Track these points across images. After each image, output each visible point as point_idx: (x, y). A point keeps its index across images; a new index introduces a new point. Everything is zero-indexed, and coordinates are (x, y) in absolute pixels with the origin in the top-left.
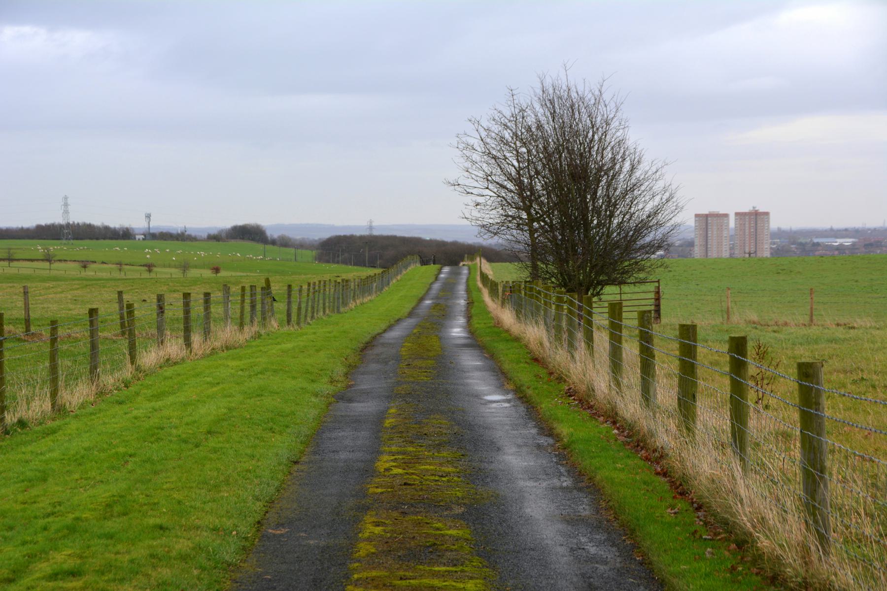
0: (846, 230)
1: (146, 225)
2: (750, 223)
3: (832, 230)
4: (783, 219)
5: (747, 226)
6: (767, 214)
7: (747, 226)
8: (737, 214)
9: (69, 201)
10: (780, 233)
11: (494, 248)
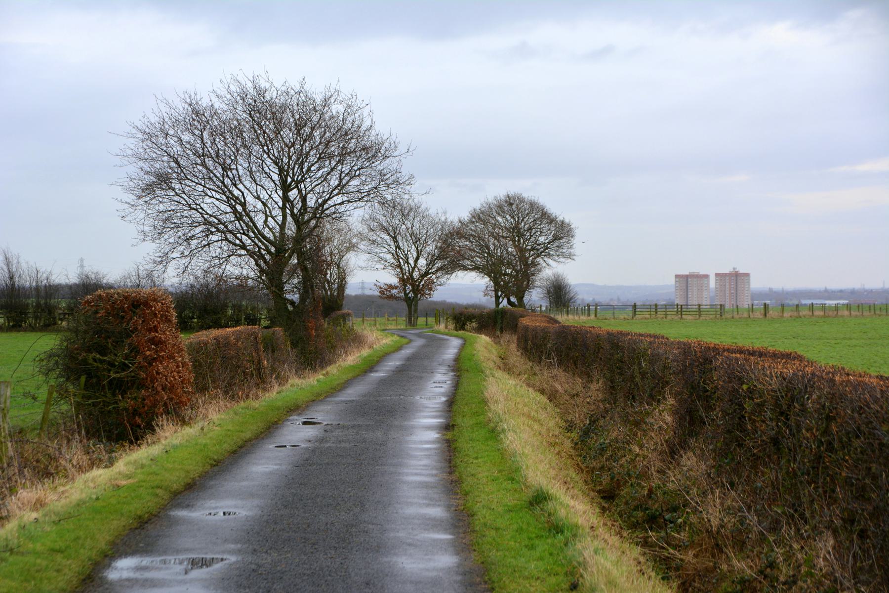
0: (841, 291)
1: (493, 306)
2: (730, 285)
3: (826, 291)
4: (759, 282)
5: (727, 286)
6: (747, 275)
7: (727, 286)
8: (717, 275)
9: (85, 263)
10: (755, 296)
11: (824, 352)
